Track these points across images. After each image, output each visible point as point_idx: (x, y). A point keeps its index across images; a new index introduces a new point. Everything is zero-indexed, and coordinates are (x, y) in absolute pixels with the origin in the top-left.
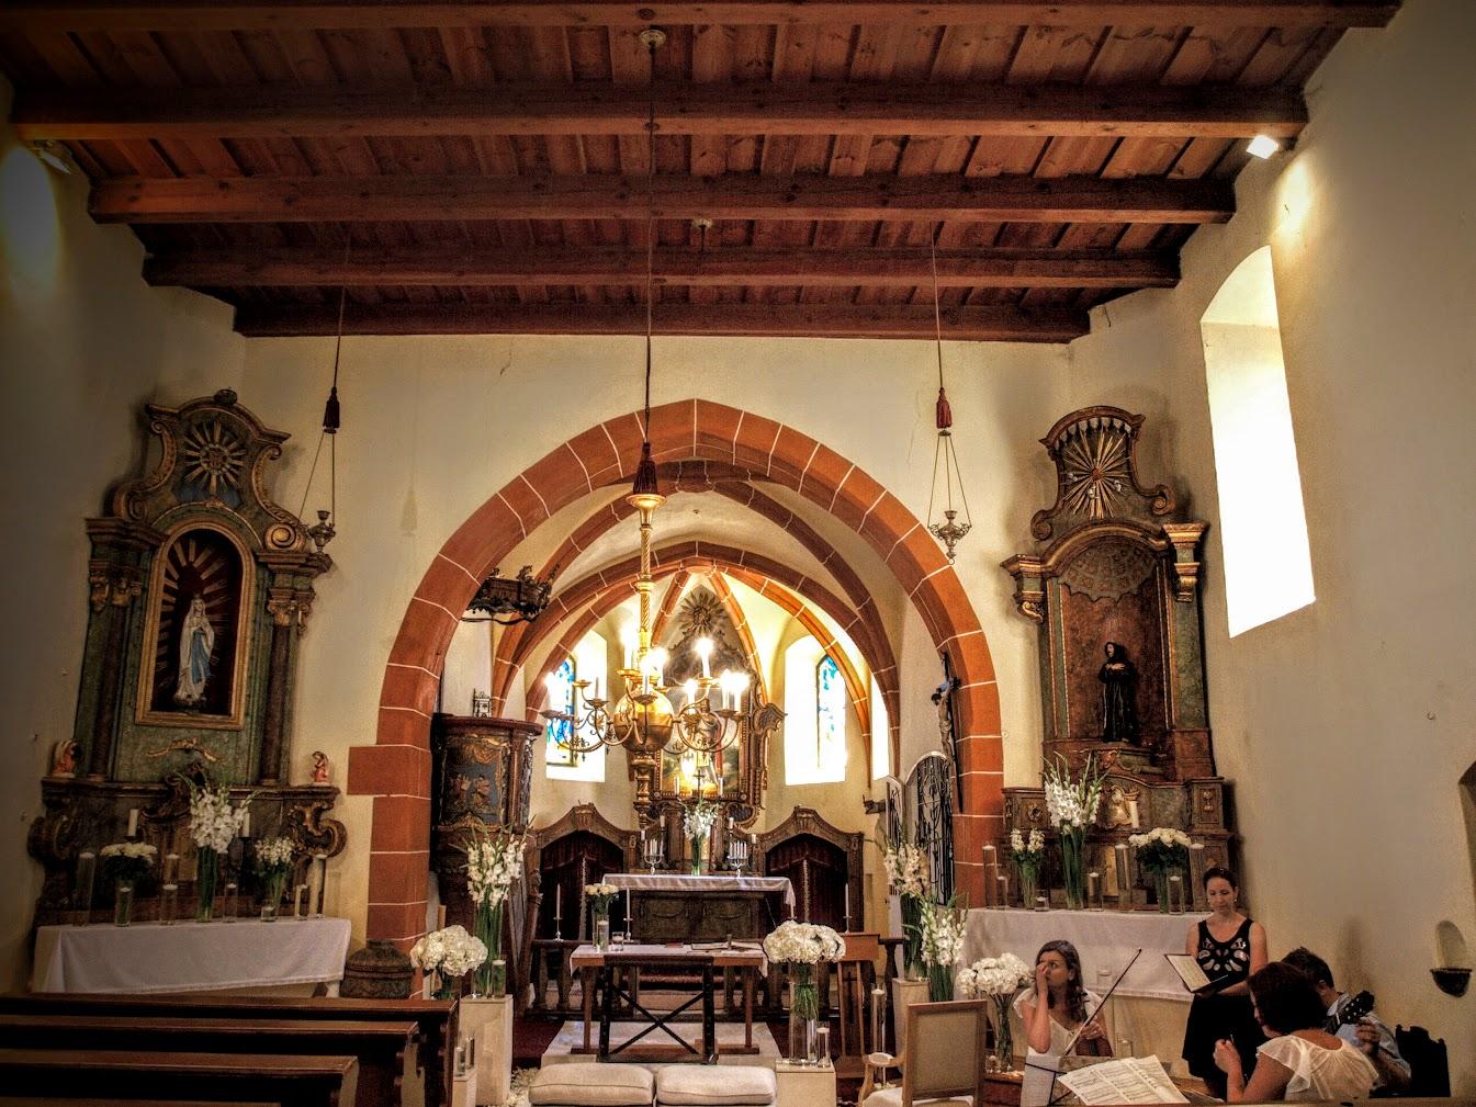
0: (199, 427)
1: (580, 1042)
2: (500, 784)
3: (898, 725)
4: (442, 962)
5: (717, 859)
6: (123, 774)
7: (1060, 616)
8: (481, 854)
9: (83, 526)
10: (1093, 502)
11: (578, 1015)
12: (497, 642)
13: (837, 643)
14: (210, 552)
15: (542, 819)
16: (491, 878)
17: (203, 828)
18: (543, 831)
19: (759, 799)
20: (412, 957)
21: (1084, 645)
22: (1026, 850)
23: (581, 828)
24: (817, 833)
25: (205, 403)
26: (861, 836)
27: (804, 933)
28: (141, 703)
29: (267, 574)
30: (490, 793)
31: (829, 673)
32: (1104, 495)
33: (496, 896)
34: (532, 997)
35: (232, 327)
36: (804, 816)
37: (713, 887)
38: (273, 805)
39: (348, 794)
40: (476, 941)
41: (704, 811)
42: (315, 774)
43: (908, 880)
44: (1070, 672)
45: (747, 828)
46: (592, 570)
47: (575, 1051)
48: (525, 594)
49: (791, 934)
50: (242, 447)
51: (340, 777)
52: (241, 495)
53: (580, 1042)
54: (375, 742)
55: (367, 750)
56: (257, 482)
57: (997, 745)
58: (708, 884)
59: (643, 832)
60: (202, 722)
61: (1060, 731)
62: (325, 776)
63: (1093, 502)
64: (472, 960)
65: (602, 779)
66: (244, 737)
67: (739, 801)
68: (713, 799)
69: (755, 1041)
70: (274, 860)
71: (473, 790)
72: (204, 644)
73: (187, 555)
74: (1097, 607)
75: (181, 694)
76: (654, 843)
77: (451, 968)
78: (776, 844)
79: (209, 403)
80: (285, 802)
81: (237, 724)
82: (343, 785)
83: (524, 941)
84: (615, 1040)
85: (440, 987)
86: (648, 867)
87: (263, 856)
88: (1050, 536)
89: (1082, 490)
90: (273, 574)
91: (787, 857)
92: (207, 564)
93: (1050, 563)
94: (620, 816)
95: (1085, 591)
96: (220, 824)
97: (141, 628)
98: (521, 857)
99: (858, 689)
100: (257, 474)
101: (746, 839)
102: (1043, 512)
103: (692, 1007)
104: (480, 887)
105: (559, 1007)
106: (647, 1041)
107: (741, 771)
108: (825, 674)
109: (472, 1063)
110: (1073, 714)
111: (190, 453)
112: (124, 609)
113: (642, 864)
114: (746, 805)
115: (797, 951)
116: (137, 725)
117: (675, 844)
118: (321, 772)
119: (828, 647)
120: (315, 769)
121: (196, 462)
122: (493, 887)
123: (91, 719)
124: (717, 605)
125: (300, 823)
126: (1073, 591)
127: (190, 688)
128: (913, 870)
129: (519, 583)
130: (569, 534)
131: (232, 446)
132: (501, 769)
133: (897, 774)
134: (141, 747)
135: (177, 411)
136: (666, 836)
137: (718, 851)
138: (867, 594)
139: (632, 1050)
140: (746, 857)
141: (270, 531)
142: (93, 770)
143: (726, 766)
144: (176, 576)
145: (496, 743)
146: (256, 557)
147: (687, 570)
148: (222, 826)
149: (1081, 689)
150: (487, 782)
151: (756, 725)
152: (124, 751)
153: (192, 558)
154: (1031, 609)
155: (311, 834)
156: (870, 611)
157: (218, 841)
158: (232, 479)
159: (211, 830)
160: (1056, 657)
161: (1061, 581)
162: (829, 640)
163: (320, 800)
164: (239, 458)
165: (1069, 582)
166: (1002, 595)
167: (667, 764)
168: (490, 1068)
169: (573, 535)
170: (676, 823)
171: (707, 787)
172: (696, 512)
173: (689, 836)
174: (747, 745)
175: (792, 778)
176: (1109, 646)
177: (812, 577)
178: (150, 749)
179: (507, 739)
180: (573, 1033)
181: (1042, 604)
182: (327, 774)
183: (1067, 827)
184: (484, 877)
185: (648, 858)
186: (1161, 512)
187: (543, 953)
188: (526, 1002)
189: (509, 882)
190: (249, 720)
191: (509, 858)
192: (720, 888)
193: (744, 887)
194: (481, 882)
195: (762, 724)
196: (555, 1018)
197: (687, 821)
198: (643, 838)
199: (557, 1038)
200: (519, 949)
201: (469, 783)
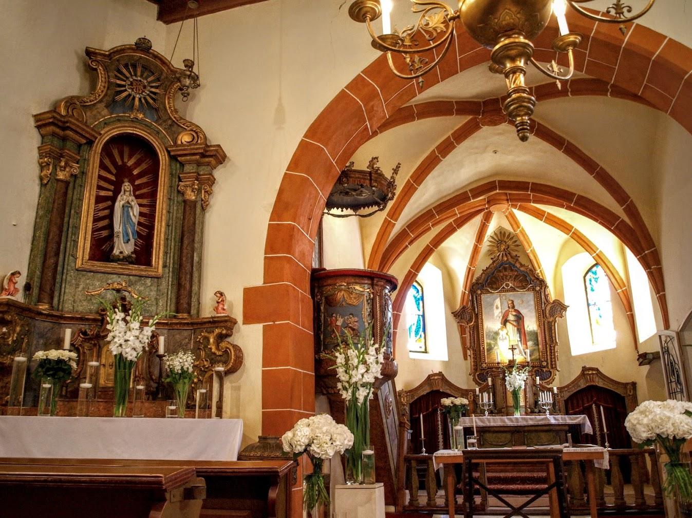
0: (126, 66)
2: (366, 320)
3: (664, 290)
4: (309, 445)
6: (68, 306)
8: (347, 359)
9: (32, 122)
13: (600, 251)
14: (139, 156)
15: (407, 384)
17: (116, 340)
18: (410, 391)
19: (555, 364)
20: (284, 442)
23: (435, 389)
24: (601, 384)
25: (129, 49)
26: (634, 384)
27: (672, 409)
28: (80, 254)
29: (178, 165)
31: (593, 280)
33: (362, 394)
35: (156, 18)
36: (590, 372)
37: (531, 423)
38: (186, 334)
39: (244, 324)
40: (343, 428)
41: (519, 371)
42: (216, 309)
48: (376, 181)
50: (158, 80)
51: (238, 314)
52: (154, 108)
54: (263, 283)
55: (256, 289)
56: (169, 103)
58: (527, 421)
60: (129, 269)
62: (224, 309)
64: (338, 443)
65: (446, 359)
66: (164, 284)
67: (541, 367)
68: (522, 366)
70: (178, 368)
71: (346, 325)
72: (131, 214)
73: (122, 158)
75: (116, 252)
77: (318, 451)
78: (572, 393)
79: (131, 48)
80: (195, 329)
81: (157, 272)
82: (239, 317)
83: (399, 455)
87: (169, 366)
90: (182, 165)
91: (580, 402)
92: (137, 164)
94: (461, 377)
96: (130, 336)
97: (81, 200)
99: (619, 281)
100: (169, 98)
104: (347, 385)
105: (428, 504)
107: (540, 346)
108: (591, 280)
111: (119, 82)
112: (67, 183)
114: (546, 369)
115: (669, 425)
116: (77, 270)
118: (221, 306)
119: (595, 254)
120: (217, 305)
121: (124, 88)
122: (359, 386)
123: (39, 261)
125: (206, 347)
127: (123, 247)
129: (370, 173)
131: (149, 79)
133: (667, 326)
134: (81, 287)
135: (107, 53)
136: (493, 390)
137: (531, 400)
140: (551, 402)
141: (180, 137)
142: (39, 300)
143: (530, 343)
144: (114, 171)
145: (361, 289)
146: (169, 152)
147: (491, 209)
148: (132, 338)
150: (356, 319)
151: (548, 315)
152: (68, 290)
153: (126, 160)
155: (214, 354)
156: (632, 211)
157: (128, 350)
158: (151, 101)
159: (122, 341)
162: (595, 250)
163: (221, 327)
164: (157, 87)
167: (489, 345)
169: (411, 177)
170: (499, 382)
171: (519, 358)
172: (495, 152)
174: (543, 329)
175: (576, 350)
178: (88, 288)
179: (370, 286)
182: (225, 308)
184: (350, 378)
185: (483, 405)
189: (373, 381)
190: (167, 270)
191: (370, 359)
192: (536, 423)
193: (553, 421)
194: (348, 382)
195: (552, 314)
197: (507, 378)
198: (477, 393)
200: (395, 461)
201: (342, 320)
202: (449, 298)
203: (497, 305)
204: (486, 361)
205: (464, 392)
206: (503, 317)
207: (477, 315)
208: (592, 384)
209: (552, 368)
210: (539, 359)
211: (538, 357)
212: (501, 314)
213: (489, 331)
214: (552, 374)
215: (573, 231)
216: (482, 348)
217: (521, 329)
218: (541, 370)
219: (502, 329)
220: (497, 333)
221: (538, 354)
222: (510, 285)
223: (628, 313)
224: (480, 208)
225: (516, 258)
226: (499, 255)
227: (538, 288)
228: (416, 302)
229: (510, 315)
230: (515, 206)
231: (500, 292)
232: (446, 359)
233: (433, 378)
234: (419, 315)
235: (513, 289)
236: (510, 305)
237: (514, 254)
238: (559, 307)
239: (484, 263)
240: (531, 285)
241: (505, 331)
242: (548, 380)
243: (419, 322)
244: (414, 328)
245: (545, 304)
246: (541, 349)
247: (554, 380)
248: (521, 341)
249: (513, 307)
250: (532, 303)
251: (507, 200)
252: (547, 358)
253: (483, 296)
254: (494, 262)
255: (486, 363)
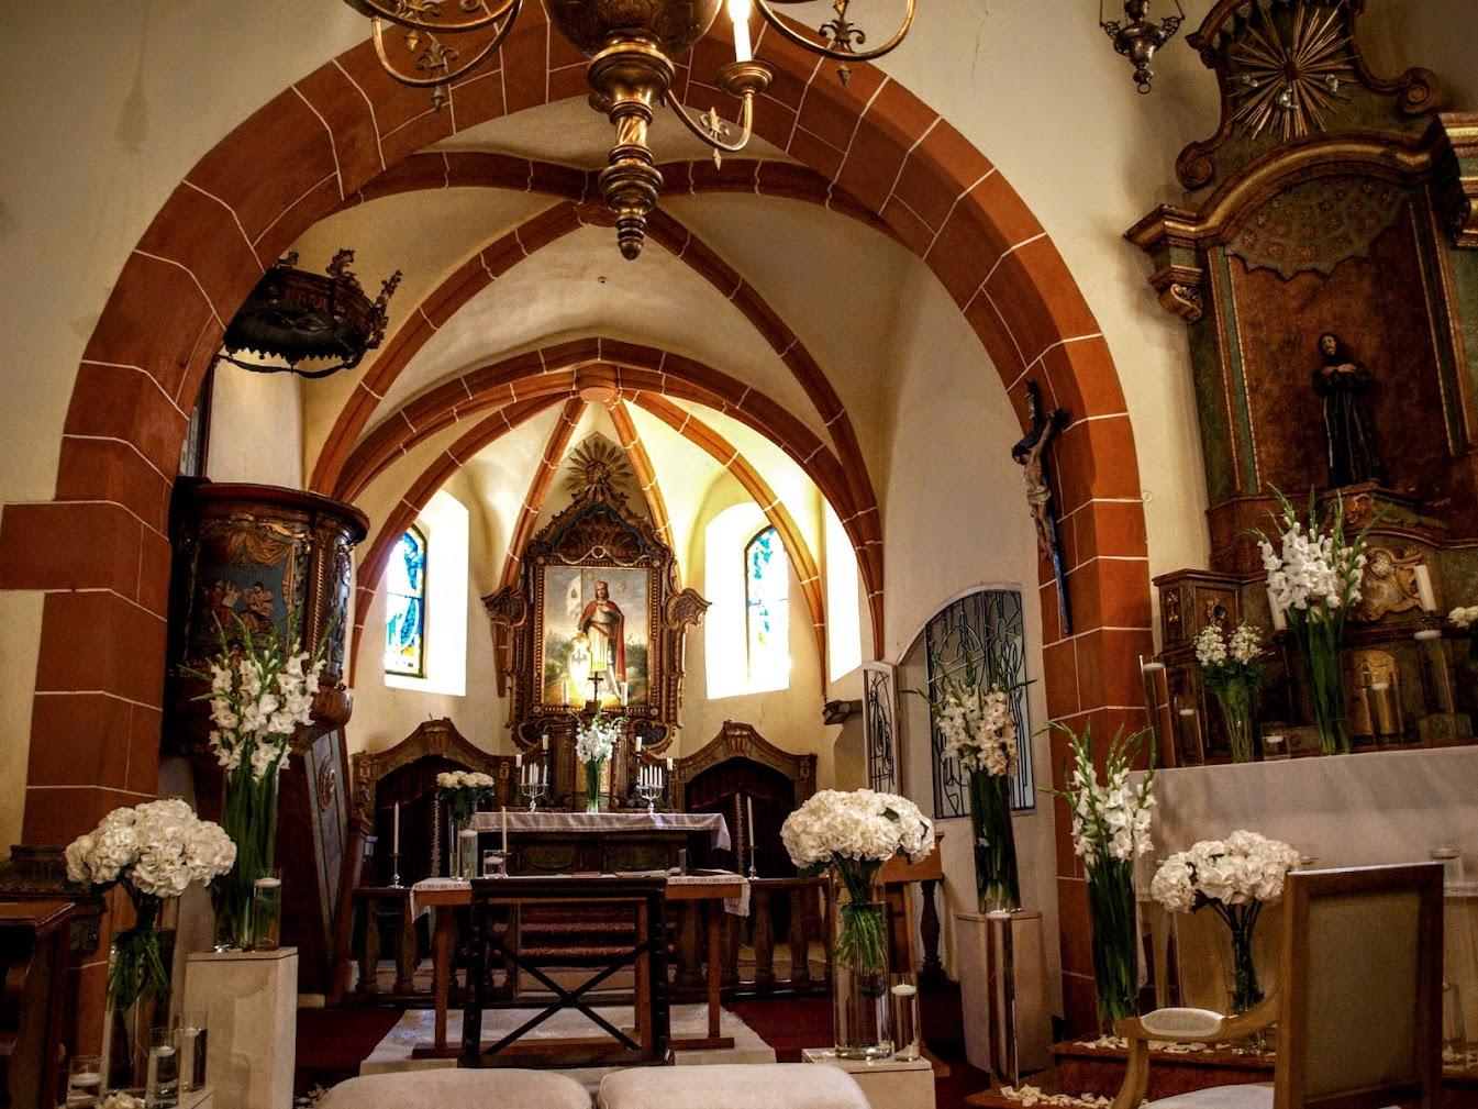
1: (429, 1038)
4: (130, 866)
5: (619, 792)
7: (1234, 306)
8: (237, 681)
10: (1287, 116)
11: (425, 1002)
12: (311, 466)
16: (254, 718)
18: (380, 756)
21: (1274, 348)
22: (1230, 658)
23: (432, 752)
26: (813, 759)
27: (864, 806)
30: (273, 614)
31: (761, 556)
32: (1308, 100)
33: (263, 758)
34: (355, 977)
36: (738, 733)
37: (618, 826)
41: (603, 725)
43: (987, 745)
44: (1253, 390)
45: (658, 753)
46: (449, 374)
47: (420, 1054)
49: (840, 809)
53: (429, 1038)
57: (1137, 513)
59: (519, 757)
61: (1245, 483)
63: (1287, 116)
64: (198, 862)
65: (462, 692)
67: (648, 717)
68: (612, 715)
69: (725, 1032)
71: (243, 608)
74: (1292, 289)
76: (534, 769)
77: (150, 879)
78: (699, 771)
84: (490, 1035)
85: (133, 924)
86: (525, 805)
88: (1211, 179)
89: (1271, 96)
93: (1214, 220)
94: (488, 731)
95: (1271, 264)
98: (313, 684)
99: (806, 562)
101: (662, 764)
102: (1195, 145)
103: (599, 985)
106: (540, 1033)
108: (756, 558)
109: (199, 1079)
110: (1263, 456)
113: (518, 800)
115: (856, 836)
117: (562, 772)
119: (769, 508)
124: (618, 459)
126: (1251, 266)
128: (994, 728)
130: (417, 305)
132: (293, 577)
133: (880, 655)
136: (551, 759)
138: (840, 406)
139: (517, 1048)
140: (661, 786)
143: (630, 671)
145: (286, 533)
149: (1274, 417)
150: (269, 595)
151: (670, 617)
154: (1181, 295)
156: (842, 432)
160: (1229, 366)
161: (1229, 252)
165: (1244, 253)
166: (1130, 280)
167: (551, 668)
168: (245, 1090)
169: (424, 305)
170: (563, 744)
171: (607, 699)
172: (602, 280)
173: (582, 758)
176: (1326, 338)
177: (758, 388)
180: (419, 1027)
181: (1202, 288)
183: (1316, 610)
185: (527, 789)
186: (1419, 109)
187: (372, 905)
188: (345, 985)
191: (289, 684)
193: (660, 825)
194: (234, 730)
196: (392, 1006)
197: (580, 738)
198: (519, 764)
199: (390, 1036)
202: (478, 569)
203: (574, 591)
204: (542, 701)
205: (492, 763)
206: (584, 616)
207: (532, 609)
208: (740, 754)
209: (668, 721)
210: (646, 701)
211: (643, 699)
212: (579, 609)
213: (555, 643)
214: (668, 733)
215: (734, 457)
216: (535, 674)
217: (616, 641)
218: (648, 724)
219: (578, 638)
220: (569, 647)
221: (643, 693)
222: (604, 551)
223: (817, 625)
224: (560, 390)
225: (621, 499)
226: (589, 489)
227: (657, 563)
228: (409, 569)
229: (598, 612)
230: (630, 396)
231: (582, 564)
232: (462, 692)
233: (430, 729)
234: (413, 598)
235: (609, 561)
236: (599, 592)
237: (618, 490)
238: (694, 604)
239: (556, 502)
240: (644, 556)
241: (585, 643)
242: (660, 744)
243: (412, 612)
244: (400, 624)
245: (667, 595)
246: (650, 684)
247: (669, 744)
248: (613, 665)
249: (606, 596)
250: (643, 591)
251: (616, 381)
252: (661, 701)
253: (548, 570)
254: (576, 503)
255: (540, 705)
